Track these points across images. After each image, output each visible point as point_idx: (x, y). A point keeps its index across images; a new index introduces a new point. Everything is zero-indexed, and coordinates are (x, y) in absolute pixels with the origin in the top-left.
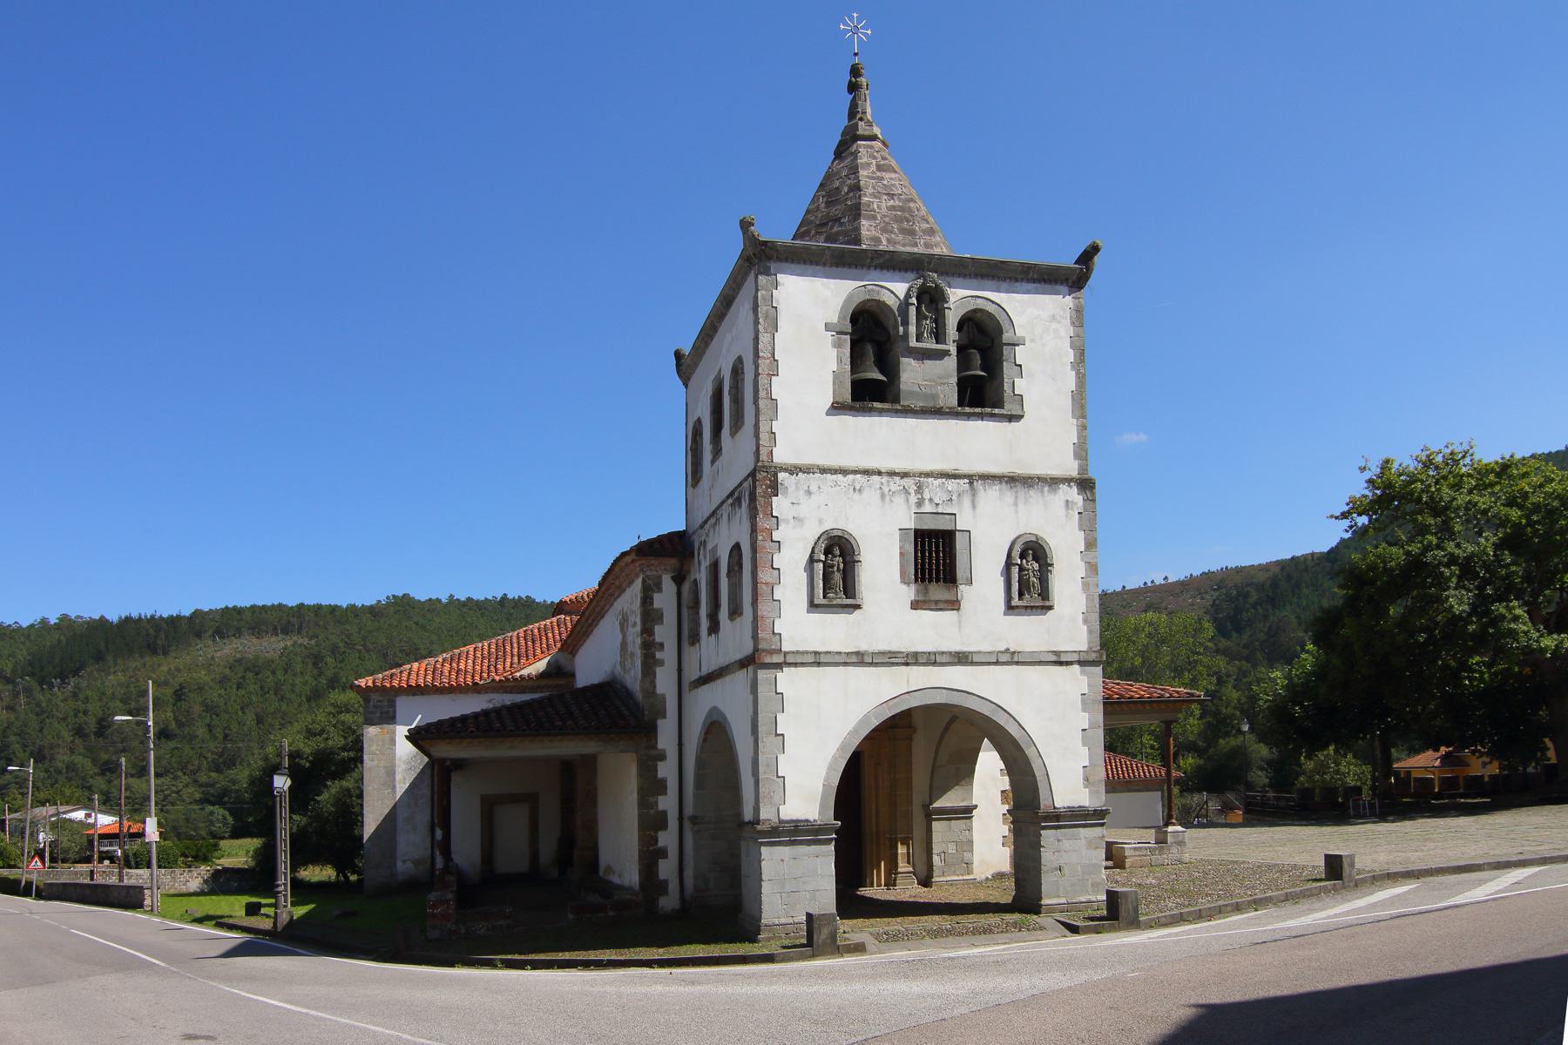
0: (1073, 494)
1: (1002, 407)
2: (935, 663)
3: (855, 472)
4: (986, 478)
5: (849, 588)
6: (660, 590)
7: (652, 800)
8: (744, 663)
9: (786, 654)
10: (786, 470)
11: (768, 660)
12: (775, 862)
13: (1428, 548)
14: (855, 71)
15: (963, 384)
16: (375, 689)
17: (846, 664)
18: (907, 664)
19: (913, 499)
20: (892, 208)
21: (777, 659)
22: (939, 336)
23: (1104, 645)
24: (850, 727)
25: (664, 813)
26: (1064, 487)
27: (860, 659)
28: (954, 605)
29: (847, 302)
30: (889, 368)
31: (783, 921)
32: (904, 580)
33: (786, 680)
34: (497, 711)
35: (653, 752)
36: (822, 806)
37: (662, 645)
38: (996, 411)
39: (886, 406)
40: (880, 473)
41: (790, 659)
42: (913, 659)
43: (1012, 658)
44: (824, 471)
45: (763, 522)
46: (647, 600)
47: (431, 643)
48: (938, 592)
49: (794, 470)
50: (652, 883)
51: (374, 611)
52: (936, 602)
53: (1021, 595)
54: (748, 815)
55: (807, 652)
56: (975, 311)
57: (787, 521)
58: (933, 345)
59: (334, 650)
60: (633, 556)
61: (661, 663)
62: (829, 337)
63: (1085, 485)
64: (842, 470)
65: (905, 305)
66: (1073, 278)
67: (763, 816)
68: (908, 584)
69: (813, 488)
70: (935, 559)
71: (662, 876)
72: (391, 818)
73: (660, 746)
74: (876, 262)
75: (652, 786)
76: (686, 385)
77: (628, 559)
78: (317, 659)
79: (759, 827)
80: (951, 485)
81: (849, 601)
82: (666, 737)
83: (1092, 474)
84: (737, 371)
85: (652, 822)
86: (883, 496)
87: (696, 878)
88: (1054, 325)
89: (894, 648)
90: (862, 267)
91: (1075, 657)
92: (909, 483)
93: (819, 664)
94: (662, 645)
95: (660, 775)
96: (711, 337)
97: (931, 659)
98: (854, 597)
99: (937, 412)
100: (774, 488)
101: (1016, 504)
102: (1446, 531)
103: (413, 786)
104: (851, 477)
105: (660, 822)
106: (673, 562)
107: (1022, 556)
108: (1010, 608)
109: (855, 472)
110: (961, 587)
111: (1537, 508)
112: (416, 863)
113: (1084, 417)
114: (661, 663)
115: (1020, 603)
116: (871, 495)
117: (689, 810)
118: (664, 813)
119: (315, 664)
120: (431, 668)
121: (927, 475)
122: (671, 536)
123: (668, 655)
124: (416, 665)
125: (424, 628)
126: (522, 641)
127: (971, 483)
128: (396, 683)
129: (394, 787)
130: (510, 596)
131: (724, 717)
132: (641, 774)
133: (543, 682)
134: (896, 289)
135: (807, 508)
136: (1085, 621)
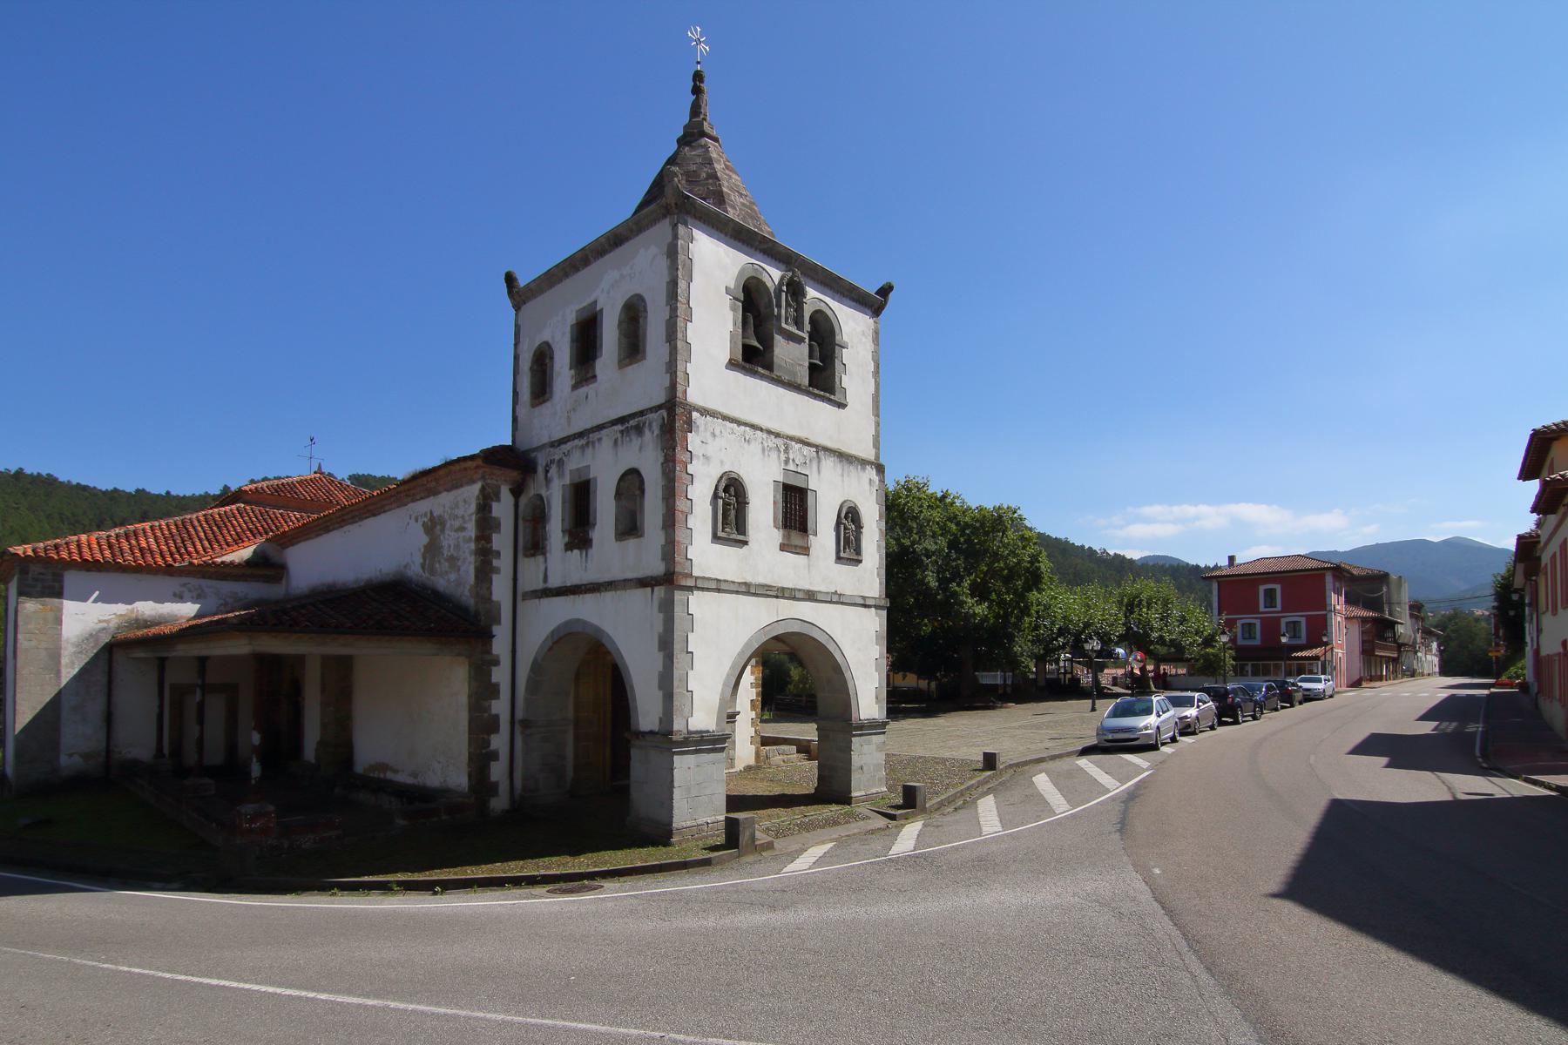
0: (871, 473)
2: (794, 598)
3: (746, 424)
4: (826, 449)
5: (741, 527)
6: (498, 500)
8: (645, 583)
11: (683, 583)
12: (685, 767)
13: (913, 543)
14: (698, 77)
16: (37, 559)
17: (737, 592)
19: (783, 457)
21: (690, 583)
22: (798, 322)
23: (887, 595)
25: (497, 717)
27: (748, 589)
28: (805, 551)
30: (768, 344)
31: (689, 824)
32: (776, 526)
41: (700, 585)
43: (837, 599)
46: (484, 508)
48: (796, 539)
49: (705, 412)
50: (481, 783)
58: (793, 329)
60: (479, 462)
61: (497, 571)
63: (880, 469)
64: (740, 425)
65: (778, 290)
66: (873, 303)
67: (676, 727)
69: (717, 432)
70: (795, 508)
71: (493, 778)
75: (483, 690)
76: (517, 308)
77: (469, 464)
80: (806, 450)
81: (741, 537)
82: (500, 646)
83: (882, 461)
85: (482, 726)
92: (779, 441)
93: (719, 590)
94: (498, 554)
100: (690, 425)
102: (921, 532)
103: (84, 671)
105: (493, 725)
106: (514, 474)
107: (726, 490)
108: (839, 559)
109: (746, 424)
111: (967, 525)
112: (86, 756)
114: (497, 571)
116: (755, 448)
117: (519, 715)
118: (497, 717)
120: (104, 542)
121: (792, 439)
122: (503, 447)
123: (504, 563)
124: (84, 537)
128: (65, 555)
129: (58, 673)
130: (28, 471)
131: (598, 630)
133: (249, 571)
134: (773, 275)
135: (713, 448)
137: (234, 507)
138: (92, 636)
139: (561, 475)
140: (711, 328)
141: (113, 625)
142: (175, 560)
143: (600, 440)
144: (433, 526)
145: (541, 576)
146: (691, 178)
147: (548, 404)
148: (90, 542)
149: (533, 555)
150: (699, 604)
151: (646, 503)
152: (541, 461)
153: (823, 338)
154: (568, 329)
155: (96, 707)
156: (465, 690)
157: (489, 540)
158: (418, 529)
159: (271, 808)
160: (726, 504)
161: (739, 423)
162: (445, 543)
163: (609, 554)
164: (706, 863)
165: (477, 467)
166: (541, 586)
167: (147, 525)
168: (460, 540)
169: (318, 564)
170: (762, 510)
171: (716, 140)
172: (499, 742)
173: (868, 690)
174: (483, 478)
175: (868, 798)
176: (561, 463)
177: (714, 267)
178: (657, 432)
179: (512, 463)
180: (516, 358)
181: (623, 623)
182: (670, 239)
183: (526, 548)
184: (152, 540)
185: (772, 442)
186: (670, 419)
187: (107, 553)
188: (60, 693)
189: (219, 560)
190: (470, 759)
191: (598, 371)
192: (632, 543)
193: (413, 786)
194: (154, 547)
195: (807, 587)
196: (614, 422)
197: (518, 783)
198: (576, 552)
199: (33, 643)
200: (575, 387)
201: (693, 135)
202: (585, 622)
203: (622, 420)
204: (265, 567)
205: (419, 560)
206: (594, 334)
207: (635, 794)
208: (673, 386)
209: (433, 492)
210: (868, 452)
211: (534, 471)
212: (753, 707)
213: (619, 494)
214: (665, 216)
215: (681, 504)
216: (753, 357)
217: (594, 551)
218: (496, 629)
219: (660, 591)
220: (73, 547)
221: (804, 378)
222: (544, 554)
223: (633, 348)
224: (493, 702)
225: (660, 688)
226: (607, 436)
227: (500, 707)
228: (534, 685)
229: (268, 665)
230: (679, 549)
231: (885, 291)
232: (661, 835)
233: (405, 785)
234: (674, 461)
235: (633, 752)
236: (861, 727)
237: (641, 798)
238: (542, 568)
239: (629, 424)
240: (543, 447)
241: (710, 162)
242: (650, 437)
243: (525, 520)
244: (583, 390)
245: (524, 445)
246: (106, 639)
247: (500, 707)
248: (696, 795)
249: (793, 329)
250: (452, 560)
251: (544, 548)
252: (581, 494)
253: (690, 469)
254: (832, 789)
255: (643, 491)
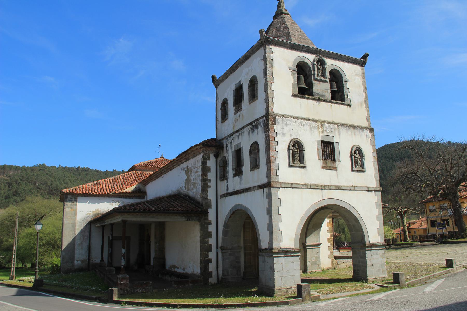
0: (367, 132)
1: (344, 101)
4: (342, 125)
6: (209, 160)
7: (206, 240)
8: (261, 187)
9: (281, 183)
10: (278, 116)
12: (280, 264)
15: (333, 93)
18: (322, 189)
19: (321, 130)
20: (299, 35)
21: (278, 185)
22: (324, 75)
23: (381, 185)
24: (304, 212)
25: (211, 245)
26: (365, 130)
27: (307, 187)
28: (335, 169)
29: (296, 60)
30: (310, 85)
32: (319, 159)
33: (283, 194)
34: (133, 205)
35: (206, 221)
36: (295, 243)
37: (210, 180)
38: (343, 103)
39: (310, 97)
40: (309, 120)
41: (283, 186)
42: (323, 188)
43: (354, 188)
44: (291, 117)
45: (271, 134)
46: (204, 163)
47: (52, 181)
48: (330, 164)
49: (282, 116)
51: (32, 169)
52: (330, 167)
53: (355, 166)
54: (264, 245)
55: (288, 183)
56: (333, 70)
57: (280, 134)
58: (322, 78)
59: (16, 181)
60: (201, 146)
61: (210, 187)
62: (290, 72)
63: (371, 130)
66: (362, 62)
67: (274, 246)
68: (321, 160)
69: (288, 123)
70: (328, 151)
71: (210, 270)
72: (73, 243)
73: (209, 219)
74: (303, 49)
76: (216, 88)
77: (198, 147)
78: (10, 185)
79: (274, 251)
80: (332, 126)
83: (372, 127)
84: (253, 82)
85: (206, 249)
86: (311, 128)
87: (223, 271)
88: (357, 77)
89: (317, 183)
90: (299, 50)
91: (373, 189)
94: (210, 180)
95: (209, 230)
96: (234, 70)
97: (329, 188)
98: (303, 163)
99: (326, 101)
100: (275, 122)
101: (352, 135)
103: (82, 231)
104: (300, 120)
105: (209, 249)
107: (355, 152)
110: (337, 162)
112: (82, 261)
113: (368, 108)
114: (210, 187)
115: (356, 169)
116: (307, 127)
117: (220, 245)
118: (211, 245)
119: (9, 187)
120: (90, 187)
121: (324, 122)
122: (212, 140)
123: (212, 184)
124: (84, 185)
125: (50, 176)
126: (122, 179)
127: (338, 126)
128: (78, 192)
129: (75, 232)
131: (246, 208)
132: (201, 230)
134: (310, 58)
135: (286, 129)
136: (375, 177)
137: (132, 172)
138: (84, 219)
139: (231, 148)
140: (282, 82)
141: (91, 215)
142: (110, 192)
143: (244, 132)
144: (188, 171)
145: (226, 188)
146: (278, 29)
147: (227, 121)
148: (85, 187)
149: (223, 180)
150: (283, 194)
151: (260, 155)
152: (225, 143)
153: (337, 78)
154: (232, 92)
155: (86, 244)
156: (199, 235)
157: (206, 175)
158: (183, 173)
159: (128, 276)
160: (293, 152)
161: (298, 118)
162: (192, 178)
163: (251, 178)
164: (287, 303)
165: (200, 148)
166: (226, 192)
167: (103, 180)
168: (196, 177)
169: (155, 190)
170: (312, 153)
171: (288, 14)
172: (212, 255)
173: (374, 228)
174: (203, 152)
175: (377, 280)
176: (231, 142)
177: (283, 60)
178: (262, 126)
179: (214, 146)
180: (216, 105)
181: (253, 203)
182: (263, 54)
183: (221, 178)
184: (104, 185)
185: (315, 124)
186: (266, 121)
187: (90, 191)
188: (75, 238)
189: (124, 191)
190: (201, 262)
191: (243, 106)
192: (256, 171)
193: (183, 273)
194: (105, 187)
195: (336, 184)
196: (248, 125)
197: (220, 273)
198: (237, 177)
199: (68, 222)
200: (235, 113)
201: (279, 14)
202: (241, 205)
203: (251, 124)
204: (139, 192)
205: (184, 185)
206: (243, 93)
207: (261, 275)
208: (267, 108)
209: (188, 159)
210: (366, 124)
211: (223, 147)
212: (329, 241)
213: (250, 153)
214: (261, 46)
215: (272, 153)
216: (304, 91)
217: (243, 176)
218: (210, 210)
219: (266, 190)
220: (81, 189)
221: (328, 96)
222: (227, 179)
223: (253, 96)
224: (209, 239)
225: (268, 230)
226: (246, 130)
227: (212, 241)
228: (225, 233)
229: (143, 228)
230: (273, 172)
231: (365, 56)
232: (268, 291)
233: (181, 273)
234: (269, 137)
235: (260, 257)
236: (371, 246)
237: (263, 276)
238: (226, 185)
239: (253, 125)
240: (225, 138)
241: (285, 22)
242: (261, 129)
243: (220, 167)
244: (238, 114)
245: (220, 138)
246: (89, 220)
247: (212, 241)
248: (286, 274)
249: (322, 78)
250: (194, 184)
251: (227, 177)
252: (238, 152)
253: (276, 139)
254: (359, 275)
255: (259, 150)
